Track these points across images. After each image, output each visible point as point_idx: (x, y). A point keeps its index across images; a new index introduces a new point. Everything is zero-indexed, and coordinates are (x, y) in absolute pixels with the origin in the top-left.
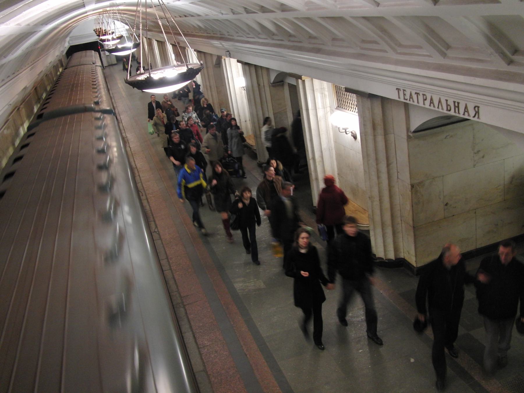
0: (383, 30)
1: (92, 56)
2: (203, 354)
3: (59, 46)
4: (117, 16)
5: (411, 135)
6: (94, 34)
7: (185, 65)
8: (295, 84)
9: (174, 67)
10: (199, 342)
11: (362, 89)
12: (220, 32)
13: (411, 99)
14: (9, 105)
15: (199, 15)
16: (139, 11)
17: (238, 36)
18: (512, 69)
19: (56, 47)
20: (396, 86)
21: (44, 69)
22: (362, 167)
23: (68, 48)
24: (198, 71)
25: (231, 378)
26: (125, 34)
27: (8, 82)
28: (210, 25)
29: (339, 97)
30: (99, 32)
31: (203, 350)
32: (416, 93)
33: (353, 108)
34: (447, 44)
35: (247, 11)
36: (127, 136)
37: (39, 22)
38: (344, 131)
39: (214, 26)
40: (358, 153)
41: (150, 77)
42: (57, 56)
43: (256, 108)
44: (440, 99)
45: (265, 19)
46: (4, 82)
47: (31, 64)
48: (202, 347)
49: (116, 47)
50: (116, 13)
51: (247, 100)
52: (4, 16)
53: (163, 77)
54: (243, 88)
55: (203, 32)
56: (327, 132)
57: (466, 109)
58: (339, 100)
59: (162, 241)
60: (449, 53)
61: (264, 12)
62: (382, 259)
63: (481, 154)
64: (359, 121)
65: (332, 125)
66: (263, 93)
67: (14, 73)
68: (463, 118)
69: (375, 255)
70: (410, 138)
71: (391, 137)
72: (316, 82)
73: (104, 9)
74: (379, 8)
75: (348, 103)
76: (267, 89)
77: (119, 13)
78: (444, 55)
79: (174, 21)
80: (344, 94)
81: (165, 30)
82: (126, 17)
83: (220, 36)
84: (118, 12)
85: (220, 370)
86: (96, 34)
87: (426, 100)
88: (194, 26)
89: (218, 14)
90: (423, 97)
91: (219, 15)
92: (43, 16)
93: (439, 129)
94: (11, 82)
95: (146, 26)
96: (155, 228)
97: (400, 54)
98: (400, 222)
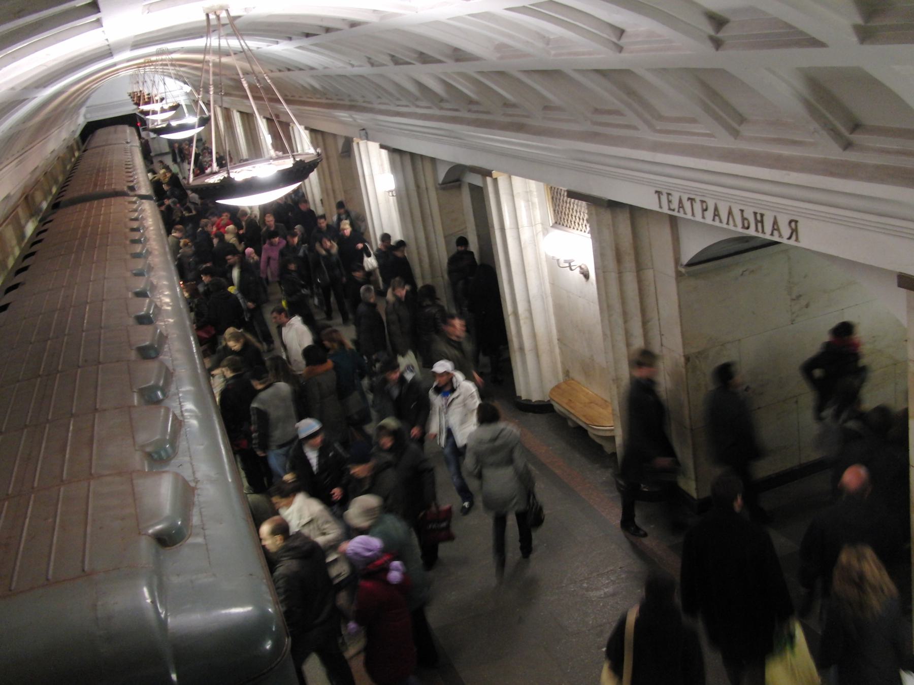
0: (631, 93)
3: (67, 123)
4: (169, 69)
5: (683, 270)
11: (596, 192)
13: (681, 210)
15: (312, 69)
18: (852, 156)
22: (598, 330)
30: (138, 99)
34: (740, 115)
35: (396, 61)
38: (567, 265)
41: (229, 177)
45: (427, 75)
50: (167, 65)
54: (391, 193)
58: (556, 212)
60: (745, 130)
66: (426, 201)
70: (681, 276)
71: (649, 274)
72: (517, 181)
74: (624, 55)
76: (433, 194)
77: (172, 65)
78: (735, 134)
84: (170, 63)
86: (134, 101)
87: (706, 210)
88: (303, 86)
97: (661, 132)
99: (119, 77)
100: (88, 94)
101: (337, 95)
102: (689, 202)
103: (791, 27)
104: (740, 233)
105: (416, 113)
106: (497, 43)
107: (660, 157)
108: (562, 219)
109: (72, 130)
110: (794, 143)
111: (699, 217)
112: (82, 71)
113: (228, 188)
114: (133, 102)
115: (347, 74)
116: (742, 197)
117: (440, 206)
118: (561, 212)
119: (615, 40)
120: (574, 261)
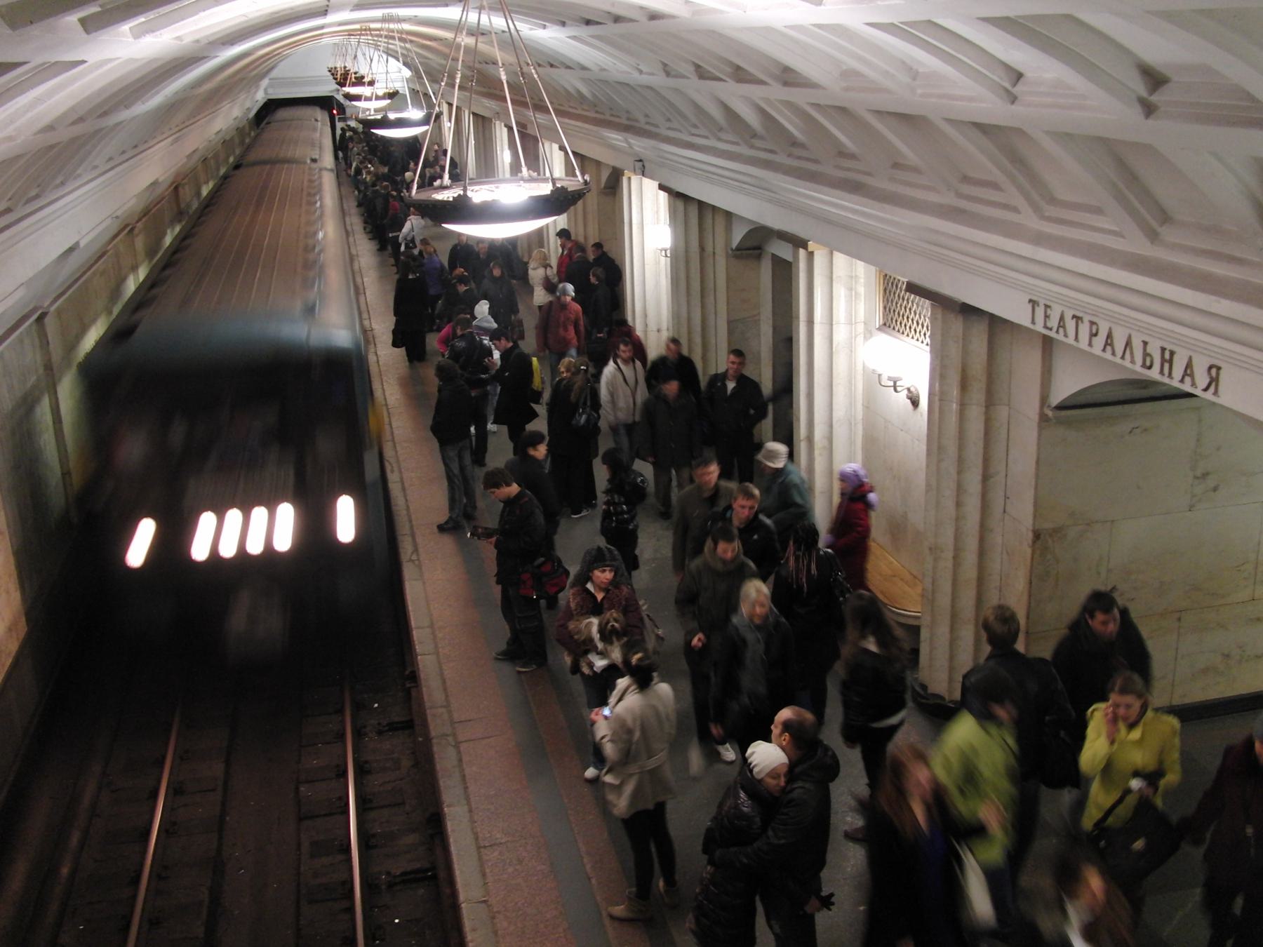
1: (315, 129)
3: (243, 97)
4: (396, 45)
5: (1050, 413)
6: (328, 78)
8: (789, 258)
9: (522, 182)
11: (947, 290)
12: (628, 112)
13: (1061, 330)
15: (584, 68)
17: (669, 129)
20: (1030, 294)
22: (922, 476)
23: (262, 104)
24: (577, 196)
26: (404, 88)
27: (120, 164)
28: (608, 94)
29: (890, 304)
30: (343, 78)
31: (489, 853)
32: (1074, 317)
33: (920, 332)
35: (702, 73)
36: (373, 327)
38: (891, 383)
39: (615, 97)
41: (465, 195)
42: (235, 119)
45: (738, 97)
46: (111, 164)
47: (177, 129)
49: (384, 116)
50: (393, 38)
51: (670, 281)
53: (493, 200)
54: (664, 252)
55: (586, 108)
56: (850, 382)
57: (1189, 370)
58: (887, 309)
60: (1167, 233)
61: (740, 80)
62: (942, 698)
63: (1211, 482)
65: (864, 367)
68: (1179, 389)
69: (927, 687)
71: (1002, 413)
72: (840, 259)
73: (363, 24)
74: (1015, 108)
77: (401, 39)
78: (1153, 236)
79: (536, 76)
80: (901, 297)
82: (417, 53)
83: (626, 122)
85: (523, 904)
86: (336, 79)
87: (1096, 335)
89: (629, 70)
91: (631, 74)
92: (230, 27)
94: (121, 168)
96: (412, 553)
97: (1050, 219)
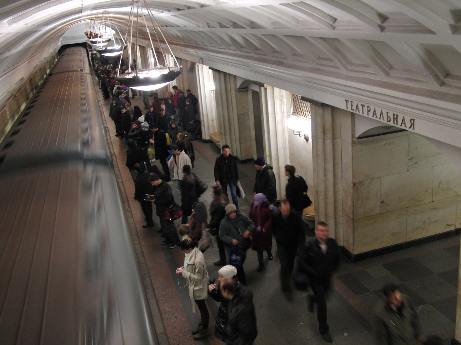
0: (337, 50)
2: (164, 318)
3: (53, 44)
4: (108, 22)
5: (355, 140)
7: (167, 68)
10: (162, 308)
11: (316, 98)
13: (357, 110)
14: (7, 92)
15: (178, 26)
16: (131, 21)
17: (211, 46)
18: (444, 89)
19: (51, 46)
20: (345, 98)
21: (39, 63)
22: (311, 166)
24: (178, 73)
25: (187, 340)
30: (90, 35)
33: (307, 114)
34: (390, 65)
35: (221, 26)
37: (42, 23)
38: (298, 133)
40: (309, 153)
41: (137, 76)
43: (223, 109)
44: (382, 111)
45: (236, 34)
47: (29, 58)
48: (163, 312)
50: (107, 20)
52: (17, 17)
54: (212, 91)
55: (180, 41)
58: (295, 107)
59: (133, 219)
60: (392, 73)
64: (312, 125)
66: (230, 97)
67: (14, 65)
70: (354, 143)
71: (338, 141)
72: (276, 90)
74: (335, 31)
75: (303, 110)
76: (233, 93)
77: (110, 20)
78: (387, 74)
79: (160, 30)
80: (299, 102)
81: (153, 38)
84: (109, 18)
86: (87, 36)
87: (370, 111)
88: (172, 35)
90: (368, 109)
93: (380, 137)
94: (10, 73)
95: (136, 33)
96: (128, 208)
97: (350, 70)
98: (342, 215)
99: (81, 23)
100: (65, 31)
101: (189, 41)
102: (362, 106)
103: (419, 23)
104: (385, 123)
105: (228, 53)
106: (273, 20)
107: (349, 83)
108: (297, 111)
109: (55, 48)
110: (416, 81)
111: (366, 114)
112: (65, 19)
113: (136, 81)
114: (87, 37)
115: (196, 31)
116: (388, 106)
117: (237, 100)
118: (297, 107)
119: (331, 23)
120: (301, 132)
